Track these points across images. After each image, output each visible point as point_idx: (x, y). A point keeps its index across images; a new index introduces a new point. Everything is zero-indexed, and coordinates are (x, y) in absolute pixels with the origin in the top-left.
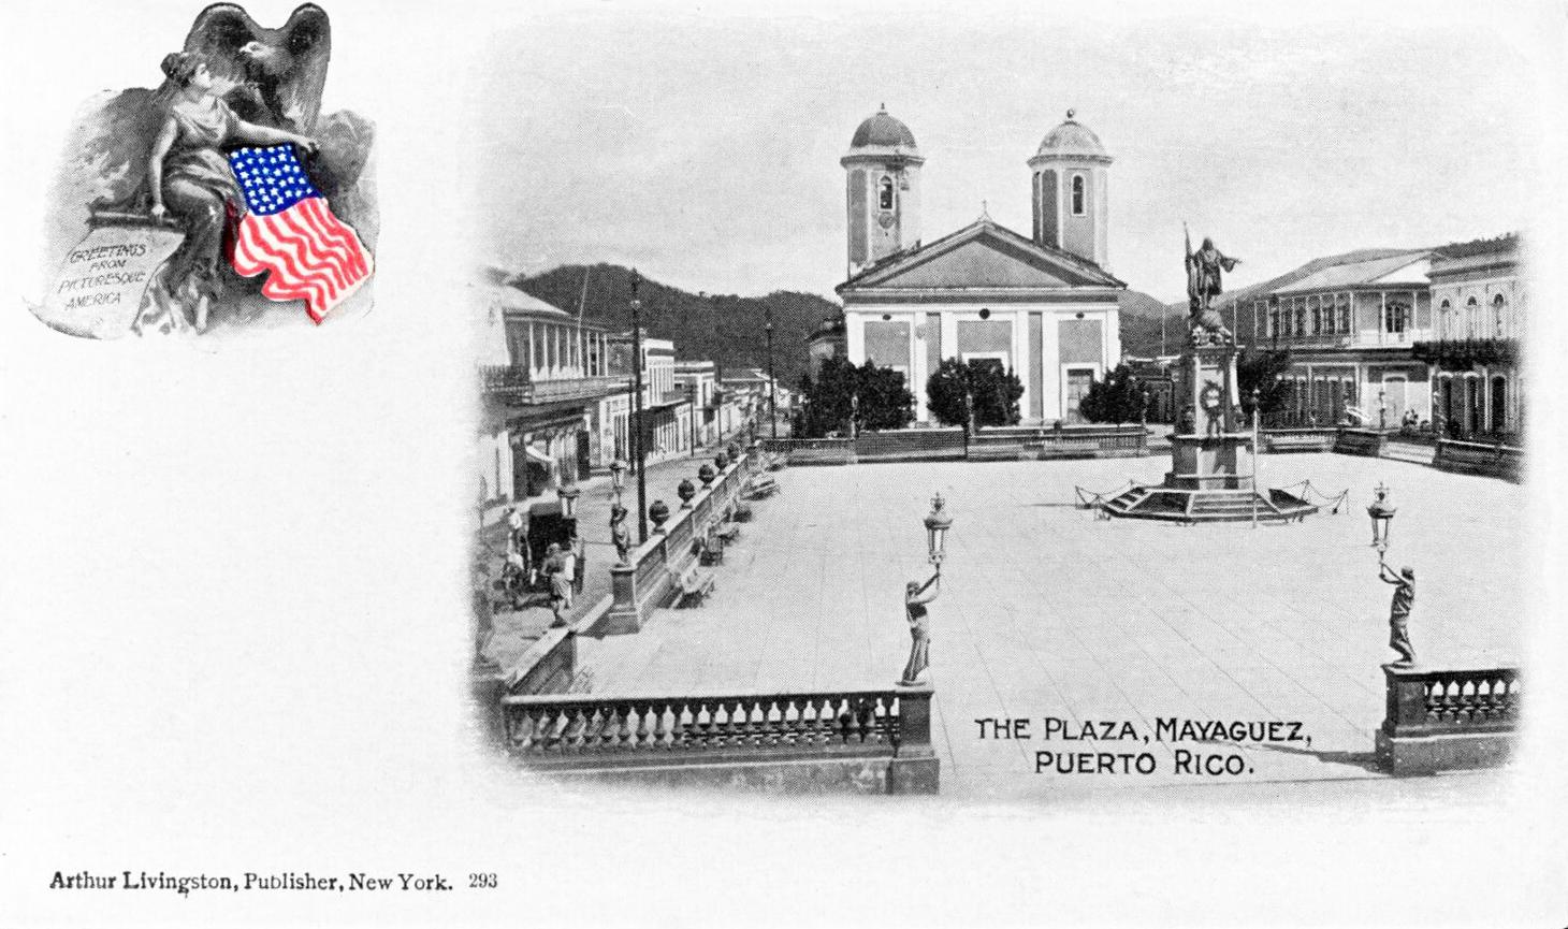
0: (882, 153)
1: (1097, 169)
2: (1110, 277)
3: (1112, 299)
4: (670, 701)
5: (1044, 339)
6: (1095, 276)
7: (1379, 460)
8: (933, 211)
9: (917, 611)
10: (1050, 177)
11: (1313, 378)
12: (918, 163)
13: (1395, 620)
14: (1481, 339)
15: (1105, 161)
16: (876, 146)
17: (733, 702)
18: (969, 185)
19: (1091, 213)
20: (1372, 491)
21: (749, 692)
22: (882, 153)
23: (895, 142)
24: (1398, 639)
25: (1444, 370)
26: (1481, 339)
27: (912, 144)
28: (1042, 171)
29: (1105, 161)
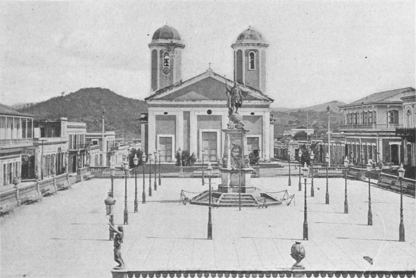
0: (166, 43)
1: (260, 49)
2: (266, 96)
3: (267, 106)
4: (313, 272)
5: (191, 124)
6: (257, 95)
7: (261, 178)
8: (191, 66)
9: (117, 238)
10: (240, 52)
11: (361, 144)
12: (182, 46)
13: (115, 251)
14: (405, 128)
15: (266, 46)
16: (162, 39)
17: (132, 273)
18: (208, 56)
19: (258, 68)
20: (107, 193)
21: (165, 269)
22: (166, 43)
23: (171, 38)
24: (117, 258)
25: (409, 141)
26: (405, 128)
27: (179, 39)
28: (236, 50)
29: (266, 46)
